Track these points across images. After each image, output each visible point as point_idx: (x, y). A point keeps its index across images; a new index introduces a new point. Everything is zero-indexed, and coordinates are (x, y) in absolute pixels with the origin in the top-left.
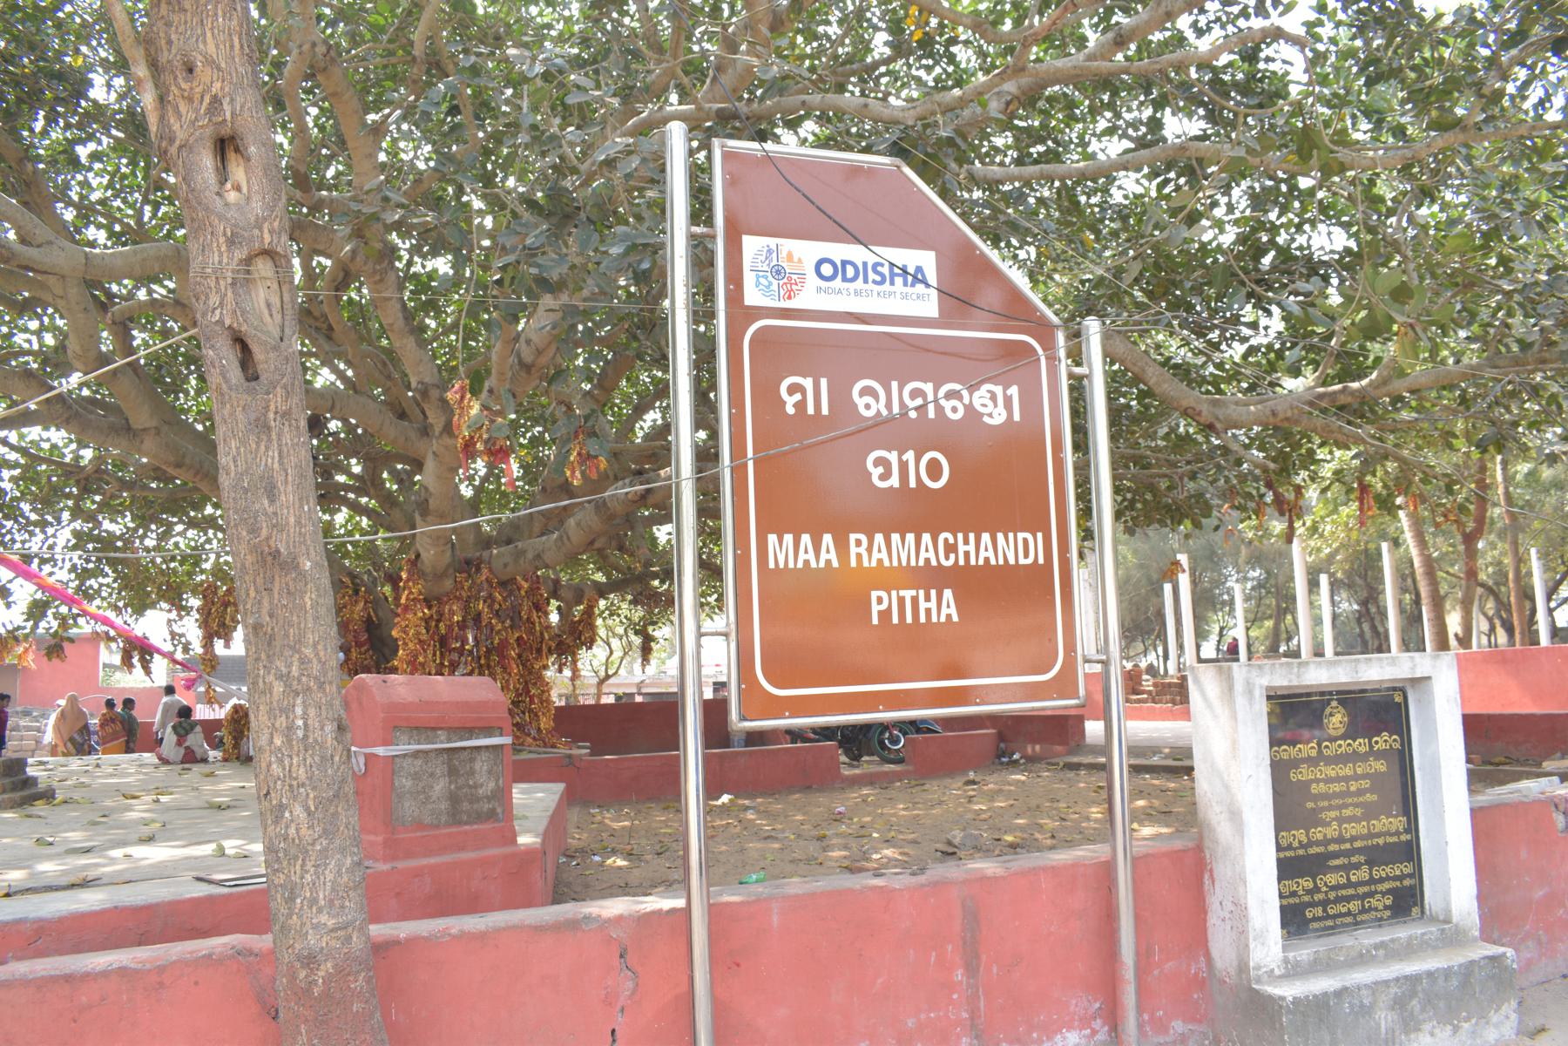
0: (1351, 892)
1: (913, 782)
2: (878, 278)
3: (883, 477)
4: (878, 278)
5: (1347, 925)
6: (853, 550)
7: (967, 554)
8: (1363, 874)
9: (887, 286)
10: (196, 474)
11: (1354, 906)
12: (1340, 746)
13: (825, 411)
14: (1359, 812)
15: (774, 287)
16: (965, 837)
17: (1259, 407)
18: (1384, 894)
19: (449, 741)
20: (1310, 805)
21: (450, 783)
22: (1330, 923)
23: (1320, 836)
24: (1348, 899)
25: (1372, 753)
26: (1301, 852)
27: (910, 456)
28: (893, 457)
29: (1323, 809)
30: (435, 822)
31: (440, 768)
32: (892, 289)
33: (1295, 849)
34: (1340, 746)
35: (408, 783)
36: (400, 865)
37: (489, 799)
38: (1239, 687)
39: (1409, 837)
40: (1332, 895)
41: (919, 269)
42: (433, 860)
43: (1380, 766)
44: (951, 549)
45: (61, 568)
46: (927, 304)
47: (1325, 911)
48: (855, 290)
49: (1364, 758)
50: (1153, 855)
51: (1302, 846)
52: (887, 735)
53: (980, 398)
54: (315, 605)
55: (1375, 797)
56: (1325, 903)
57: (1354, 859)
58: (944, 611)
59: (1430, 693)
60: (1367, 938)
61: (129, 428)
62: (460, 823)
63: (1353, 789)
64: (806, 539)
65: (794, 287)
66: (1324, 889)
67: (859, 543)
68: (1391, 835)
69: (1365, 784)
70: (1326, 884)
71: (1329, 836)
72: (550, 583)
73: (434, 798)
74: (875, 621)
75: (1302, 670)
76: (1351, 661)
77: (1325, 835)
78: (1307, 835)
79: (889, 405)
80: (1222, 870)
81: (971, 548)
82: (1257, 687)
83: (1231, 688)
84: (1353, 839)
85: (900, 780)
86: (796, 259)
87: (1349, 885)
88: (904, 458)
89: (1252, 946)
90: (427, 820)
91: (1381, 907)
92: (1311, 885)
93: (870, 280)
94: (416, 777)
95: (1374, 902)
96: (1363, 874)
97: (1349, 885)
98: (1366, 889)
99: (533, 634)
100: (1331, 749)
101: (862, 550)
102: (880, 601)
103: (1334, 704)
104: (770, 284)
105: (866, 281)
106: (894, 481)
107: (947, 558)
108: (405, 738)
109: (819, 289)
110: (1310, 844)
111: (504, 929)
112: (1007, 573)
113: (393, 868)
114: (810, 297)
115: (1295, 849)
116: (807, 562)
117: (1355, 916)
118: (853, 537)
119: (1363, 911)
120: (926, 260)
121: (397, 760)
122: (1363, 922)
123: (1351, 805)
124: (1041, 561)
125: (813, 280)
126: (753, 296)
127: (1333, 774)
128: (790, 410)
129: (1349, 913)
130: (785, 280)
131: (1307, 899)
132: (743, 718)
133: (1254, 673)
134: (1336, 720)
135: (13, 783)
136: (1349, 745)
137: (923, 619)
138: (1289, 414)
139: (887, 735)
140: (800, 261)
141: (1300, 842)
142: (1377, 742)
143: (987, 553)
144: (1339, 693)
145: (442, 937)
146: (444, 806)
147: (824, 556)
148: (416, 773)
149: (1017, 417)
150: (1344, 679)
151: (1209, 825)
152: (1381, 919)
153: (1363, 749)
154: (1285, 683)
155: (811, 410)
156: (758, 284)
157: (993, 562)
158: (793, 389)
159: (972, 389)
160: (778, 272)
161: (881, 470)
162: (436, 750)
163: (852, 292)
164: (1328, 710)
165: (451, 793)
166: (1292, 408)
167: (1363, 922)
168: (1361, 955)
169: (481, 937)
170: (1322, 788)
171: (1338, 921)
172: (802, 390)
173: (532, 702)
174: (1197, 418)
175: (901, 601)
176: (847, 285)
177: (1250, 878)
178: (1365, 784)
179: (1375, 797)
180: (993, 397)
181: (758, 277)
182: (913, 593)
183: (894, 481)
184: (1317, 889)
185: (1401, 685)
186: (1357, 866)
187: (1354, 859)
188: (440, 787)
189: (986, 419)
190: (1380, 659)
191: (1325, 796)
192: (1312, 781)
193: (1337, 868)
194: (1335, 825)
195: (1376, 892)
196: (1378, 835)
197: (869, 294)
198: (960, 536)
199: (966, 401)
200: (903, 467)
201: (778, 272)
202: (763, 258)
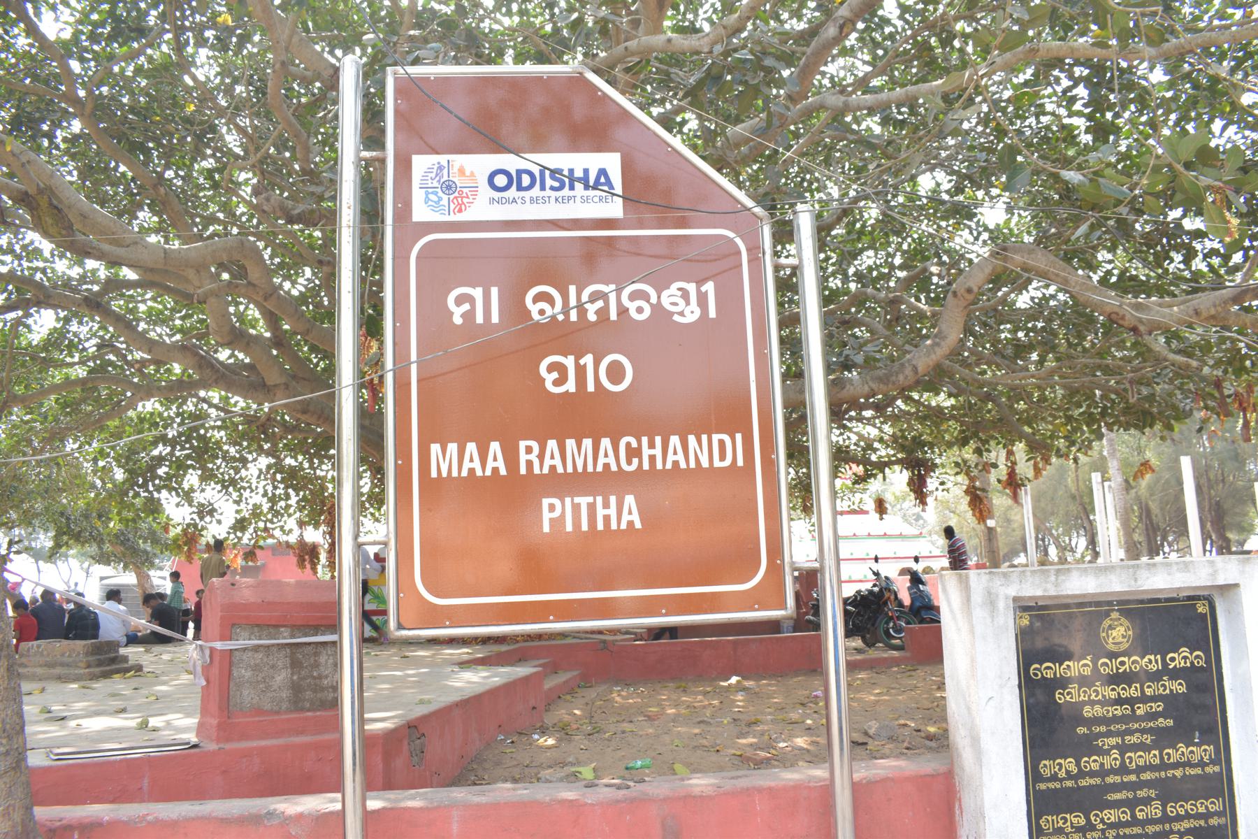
1: (909, 668)
2: (556, 184)
3: (557, 383)
4: (556, 184)
6: (523, 457)
7: (652, 459)
8: (1155, 810)
9: (566, 192)
10: (319, 418)
12: (1122, 663)
13: (495, 319)
14: (1148, 739)
15: (445, 201)
16: (880, 728)
17: (1182, 307)
19: (293, 636)
20: (1081, 730)
21: (292, 674)
23: (1095, 766)
25: (1167, 672)
26: (1069, 784)
27: (588, 360)
28: (569, 362)
30: (276, 708)
31: (281, 660)
32: (571, 193)
34: (1122, 663)
35: (248, 674)
36: (227, 746)
38: (977, 596)
39: (1217, 769)
41: (602, 172)
42: (263, 743)
44: (633, 453)
45: (257, 493)
46: (615, 209)
48: (532, 199)
49: (1156, 677)
50: (892, 780)
51: (1070, 776)
52: (891, 625)
53: (670, 297)
55: (1170, 723)
57: (1141, 794)
59: (1238, 602)
61: (264, 385)
62: (302, 710)
64: (471, 447)
65: (465, 200)
66: (1101, 826)
67: (529, 450)
69: (1158, 707)
70: (1102, 821)
71: (1107, 766)
73: (275, 687)
74: (546, 529)
75: (1062, 578)
77: (1102, 765)
78: (1078, 764)
79: (566, 311)
80: (968, 801)
81: (658, 452)
82: (1001, 597)
83: (968, 599)
84: (1140, 770)
85: (898, 665)
86: (468, 173)
88: (582, 362)
90: (268, 707)
92: (1082, 821)
93: (548, 186)
94: (256, 668)
96: (1155, 810)
97: (1135, 822)
101: (533, 457)
102: (552, 508)
103: (1115, 615)
104: (440, 199)
105: (543, 188)
106: (570, 386)
107: (629, 463)
108: (246, 634)
109: (492, 200)
111: (193, 819)
113: (220, 749)
114: (483, 207)
115: (1061, 780)
116: (472, 471)
118: (523, 444)
120: (612, 162)
121: (237, 653)
123: (1137, 730)
124: (740, 463)
125: (486, 192)
126: (421, 212)
128: (458, 320)
130: (456, 194)
132: (783, 606)
133: (998, 582)
135: (98, 660)
137: (600, 527)
138: (1213, 312)
139: (891, 625)
140: (472, 174)
141: (1068, 772)
142: (1173, 659)
143: (676, 456)
144: (1120, 603)
145: (141, 822)
146: (285, 694)
147: (490, 464)
148: (256, 665)
149: (712, 313)
151: (957, 749)
153: (1153, 668)
154: (1039, 593)
155: (480, 319)
156: (427, 200)
158: (459, 301)
161: (555, 375)
162: (278, 645)
163: (528, 200)
164: (1106, 623)
166: (1215, 306)
169: (173, 825)
170: (1098, 711)
172: (470, 299)
174: (1121, 322)
175: (576, 508)
176: (522, 194)
177: (989, 813)
178: (1158, 707)
179: (1170, 723)
180: (685, 295)
181: (427, 194)
182: (590, 499)
183: (570, 386)
185: (1206, 593)
186: (1147, 801)
187: (1141, 794)
188: (281, 677)
189: (676, 318)
192: (1084, 703)
193: (1117, 805)
194: (1115, 754)
196: (1176, 765)
197: (545, 200)
198: (645, 440)
199: (654, 300)
200: (581, 371)
201: (449, 187)
202: (433, 175)
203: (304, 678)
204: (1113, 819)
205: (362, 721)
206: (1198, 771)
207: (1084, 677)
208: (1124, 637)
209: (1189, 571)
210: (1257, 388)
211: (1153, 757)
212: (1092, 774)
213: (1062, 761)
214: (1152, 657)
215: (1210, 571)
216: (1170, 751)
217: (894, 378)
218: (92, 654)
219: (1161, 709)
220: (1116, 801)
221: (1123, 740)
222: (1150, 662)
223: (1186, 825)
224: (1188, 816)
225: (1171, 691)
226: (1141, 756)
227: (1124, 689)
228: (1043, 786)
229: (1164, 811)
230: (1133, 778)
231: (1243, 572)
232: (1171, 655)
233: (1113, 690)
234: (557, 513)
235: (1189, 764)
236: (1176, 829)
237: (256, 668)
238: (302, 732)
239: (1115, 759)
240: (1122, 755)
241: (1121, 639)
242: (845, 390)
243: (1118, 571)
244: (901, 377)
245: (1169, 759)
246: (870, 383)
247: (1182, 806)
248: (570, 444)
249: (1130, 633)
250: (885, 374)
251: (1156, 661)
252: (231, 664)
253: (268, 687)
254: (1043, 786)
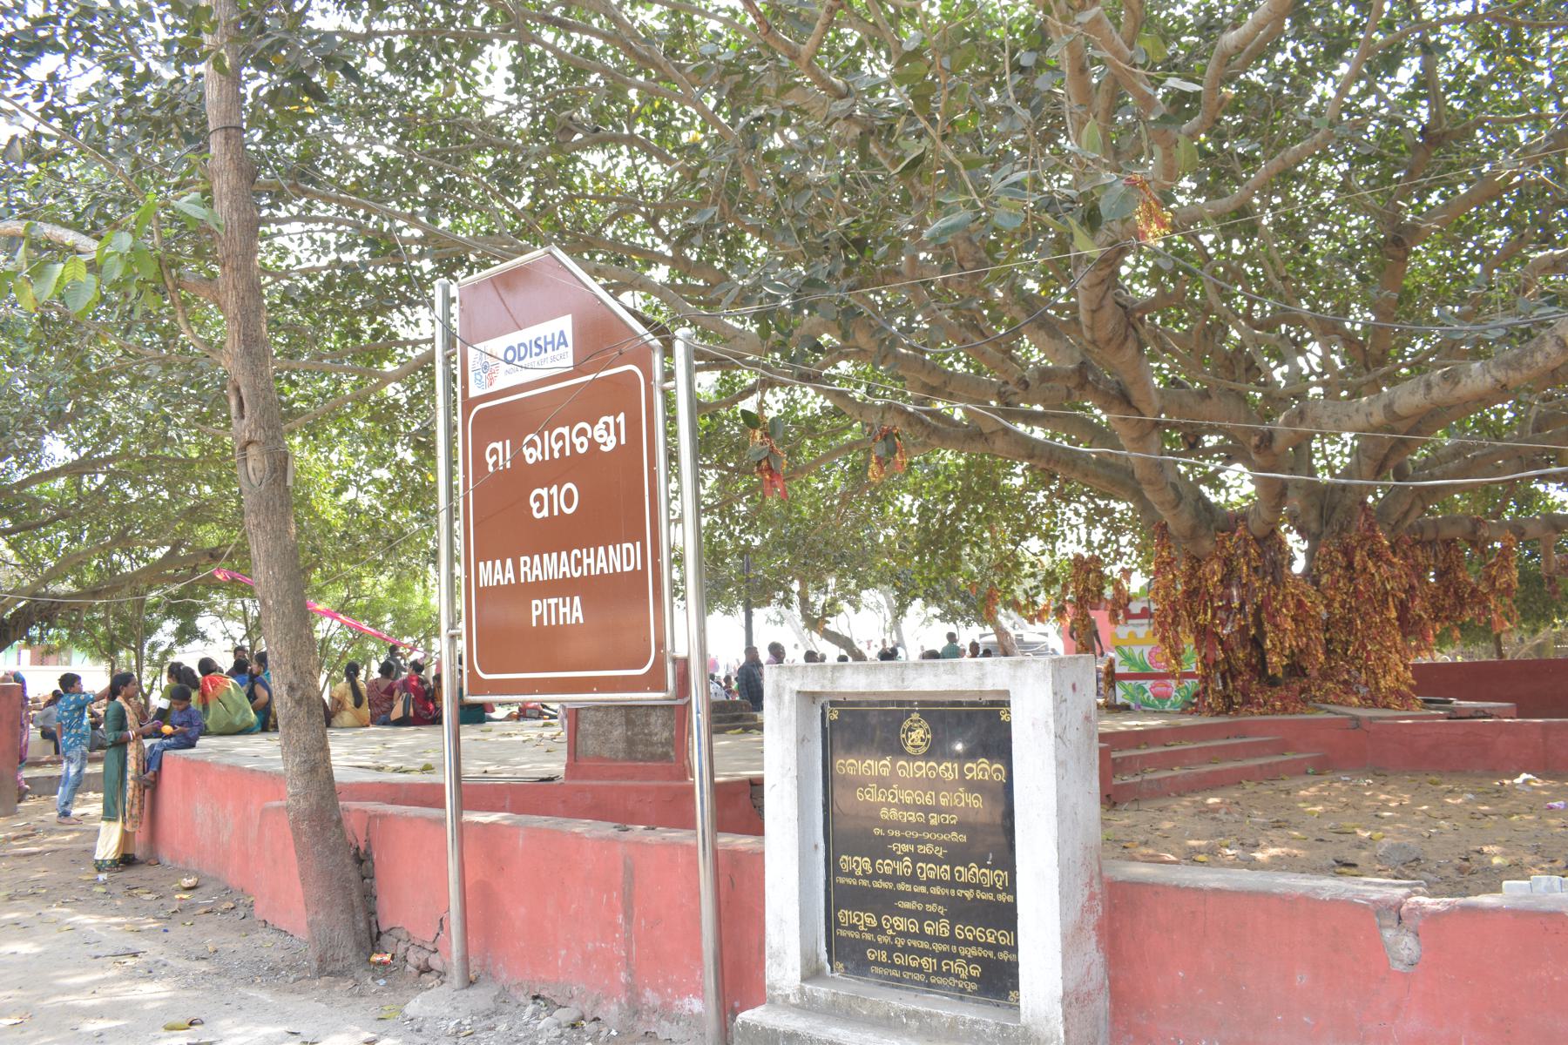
0: (924, 945)
5: (918, 983)
6: (523, 569)
12: (920, 768)
14: (940, 852)
18: (969, 961)
22: (895, 973)
23: (889, 871)
24: (922, 953)
26: (864, 883)
27: (554, 489)
29: (894, 839)
31: (618, 719)
34: (920, 768)
37: (663, 745)
40: (900, 942)
43: (975, 802)
44: (579, 562)
47: (890, 957)
53: (598, 432)
56: (891, 949)
57: (931, 908)
61: (981, 434)
62: (636, 759)
63: (934, 822)
66: (890, 932)
68: (983, 889)
71: (899, 873)
77: (894, 870)
78: (873, 865)
79: (543, 453)
84: (930, 883)
90: (606, 755)
91: (963, 975)
94: (598, 724)
95: (955, 967)
96: (942, 927)
97: (921, 935)
98: (945, 948)
99: (1374, 585)
101: (527, 569)
103: (915, 716)
106: (545, 513)
110: (875, 876)
112: (616, 577)
115: (858, 878)
118: (523, 559)
119: (938, 972)
122: (936, 986)
123: (929, 841)
126: (474, 392)
127: (909, 800)
131: (869, 937)
134: (918, 735)
136: (932, 768)
141: (864, 871)
142: (971, 770)
144: (922, 703)
146: (621, 746)
149: (623, 442)
150: (885, 688)
152: (963, 990)
158: (494, 451)
159: (593, 424)
164: (907, 724)
167: (936, 986)
168: (888, 1017)
170: (894, 814)
171: (907, 975)
173: (1368, 658)
175: (549, 606)
184: (880, 930)
186: (935, 917)
187: (931, 908)
188: (618, 732)
190: (934, 666)
191: (897, 825)
192: (883, 805)
194: (907, 861)
195: (958, 955)
196: (967, 886)
205: (712, 776)
206: (990, 896)
207: (884, 778)
211: (944, 872)
212: (885, 878)
223: (973, 952)
224: (975, 943)
228: (841, 880)
229: (952, 931)
230: (923, 889)
231: (1013, 677)
232: (969, 765)
237: (598, 724)
240: (914, 863)
244: (1539, 357)
246: (1494, 372)
248: (546, 556)
253: (607, 740)
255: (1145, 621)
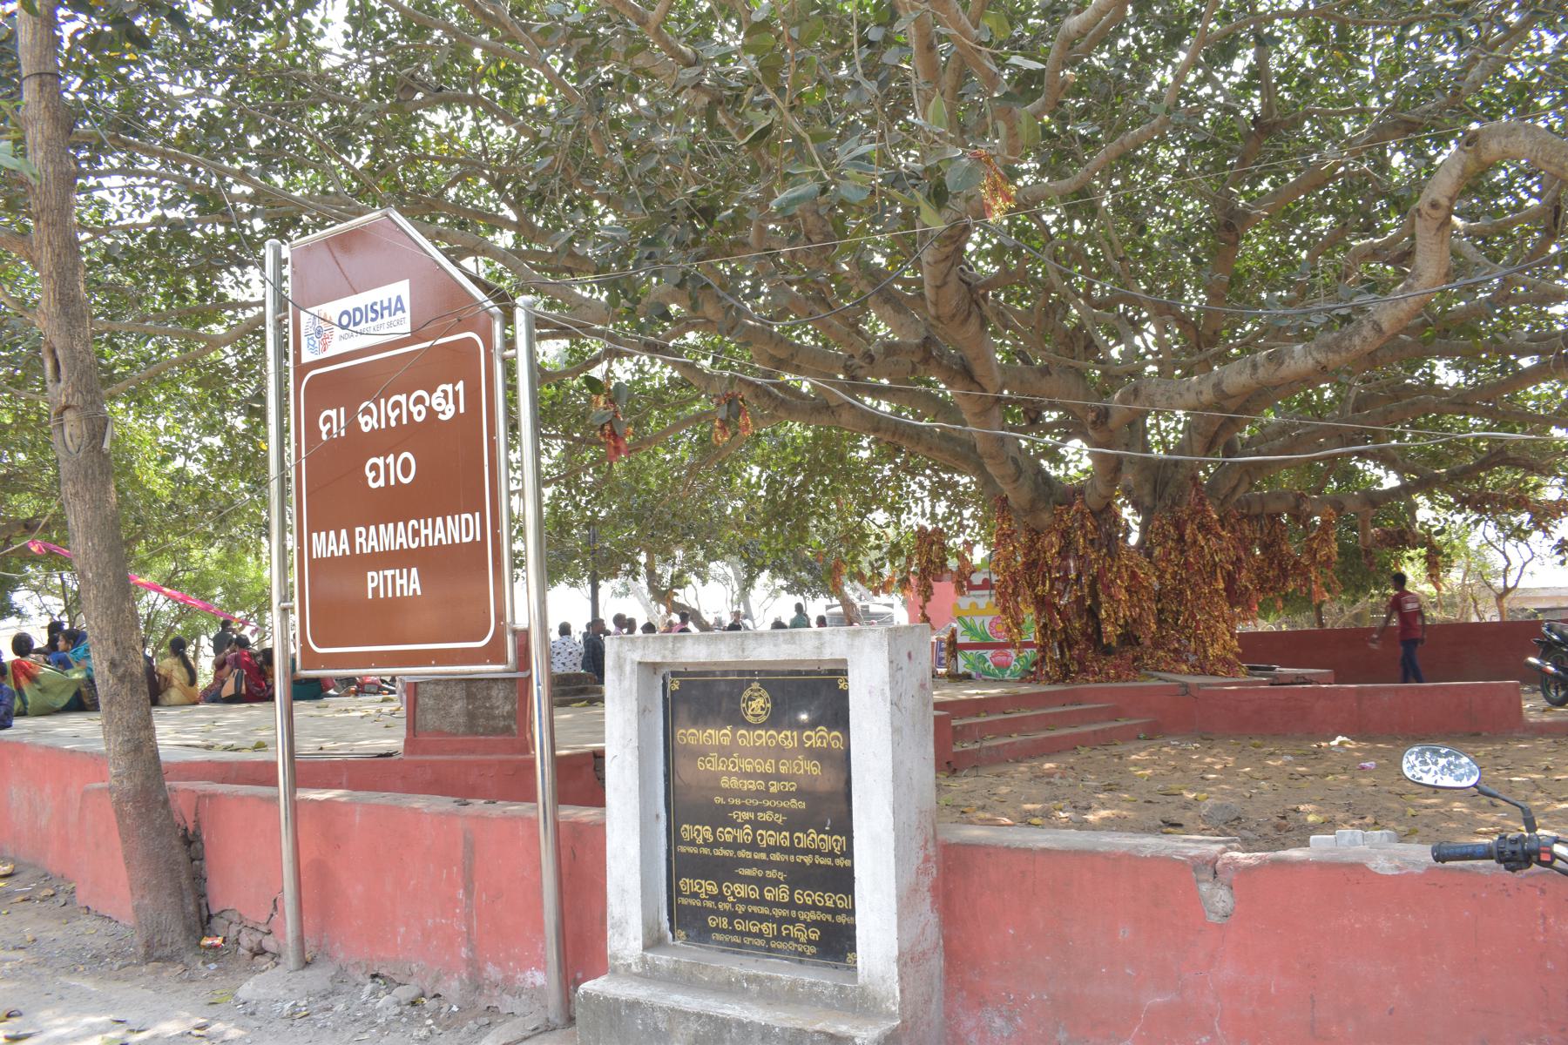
0: (764, 910)
6: (358, 540)
11: (768, 928)
12: (760, 737)
14: (779, 819)
18: (808, 925)
22: (736, 939)
23: (729, 838)
24: (762, 919)
26: (705, 851)
27: (391, 459)
29: (734, 807)
31: (459, 692)
33: (699, 846)
34: (760, 737)
40: (740, 909)
44: (416, 533)
47: (730, 923)
49: (791, 755)
53: (436, 400)
54: (96, 597)
56: (732, 916)
57: (771, 874)
58: (412, 586)
60: (784, 972)
61: (828, 407)
62: (476, 734)
63: (773, 790)
66: (731, 899)
67: (361, 533)
68: (822, 855)
71: (740, 840)
72: (1291, 498)
74: (370, 596)
76: (737, 637)
77: (735, 838)
78: (714, 833)
79: (379, 421)
82: (628, 662)
84: (770, 849)
87: (762, 901)
89: (609, 933)
90: (447, 729)
91: (803, 939)
94: (437, 698)
95: (794, 931)
96: (782, 893)
97: (762, 901)
98: (784, 913)
100: (747, 738)
101: (362, 540)
103: (755, 686)
106: (381, 483)
110: (716, 844)
115: (699, 846)
117: (768, 941)
118: (358, 530)
119: (778, 937)
123: (769, 808)
124: (478, 538)
126: (307, 357)
127: (749, 768)
129: (760, 935)
131: (710, 904)
134: (757, 704)
136: (771, 737)
142: (809, 738)
144: (760, 672)
146: (461, 720)
147: (342, 547)
149: (462, 410)
150: (726, 657)
152: (802, 954)
157: (444, 542)
159: (431, 392)
160: (319, 332)
161: (374, 474)
164: (747, 694)
165: (468, 710)
168: (729, 983)
170: (734, 783)
171: (747, 940)
175: (385, 578)
178: (791, 786)
179: (802, 805)
182: (392, 572)
186: (775, 883)
187: (771, 874)
188: (458, 706)
189: (441, 417)
192: (723, 773)
194: (748, 828)
195: (797, 920)
196: (806, 851)
198: (422, 521)
199: (427, 404)
203: (477, 708)
204: (742, 894)
208: (762, 709)
209: (794, 643)
210: (1, 543)
211: (783, 838)
212: (726, 845)
213: (764, 832)
214: (789, 733)
215: (817, 643)
216: (801, 835)
217: (1347, 342)
218: (558, 685)
219: (794, 789)
220: (746, 877)
221: (756, 816)
222: (786, 737)
223: (812, 916)
224: (814, 907)
225: (806, 771)
226: (771, 836)
227: (759, 763)
228: (683, 849)
230: (763, 856)
231: (851, 646)
233: (749, 763)
234: (375, 584)
235: (818, 852)
236: (802, 918)
237: (437, 698)
238: (473, 752)
239: (748, 834)
241: (759, 712)
242: (1284, 366)
243: (728, 639)
244: (1357, 341)
245: (799, 843)
246: (1315, 354)
247: (809, 895)
248: (382, 527)
249: (769, 705)
250: (1335, 339)
251: (793, 738)
252: (416, 693)
254: (683, 849)
255: (987, 592)
